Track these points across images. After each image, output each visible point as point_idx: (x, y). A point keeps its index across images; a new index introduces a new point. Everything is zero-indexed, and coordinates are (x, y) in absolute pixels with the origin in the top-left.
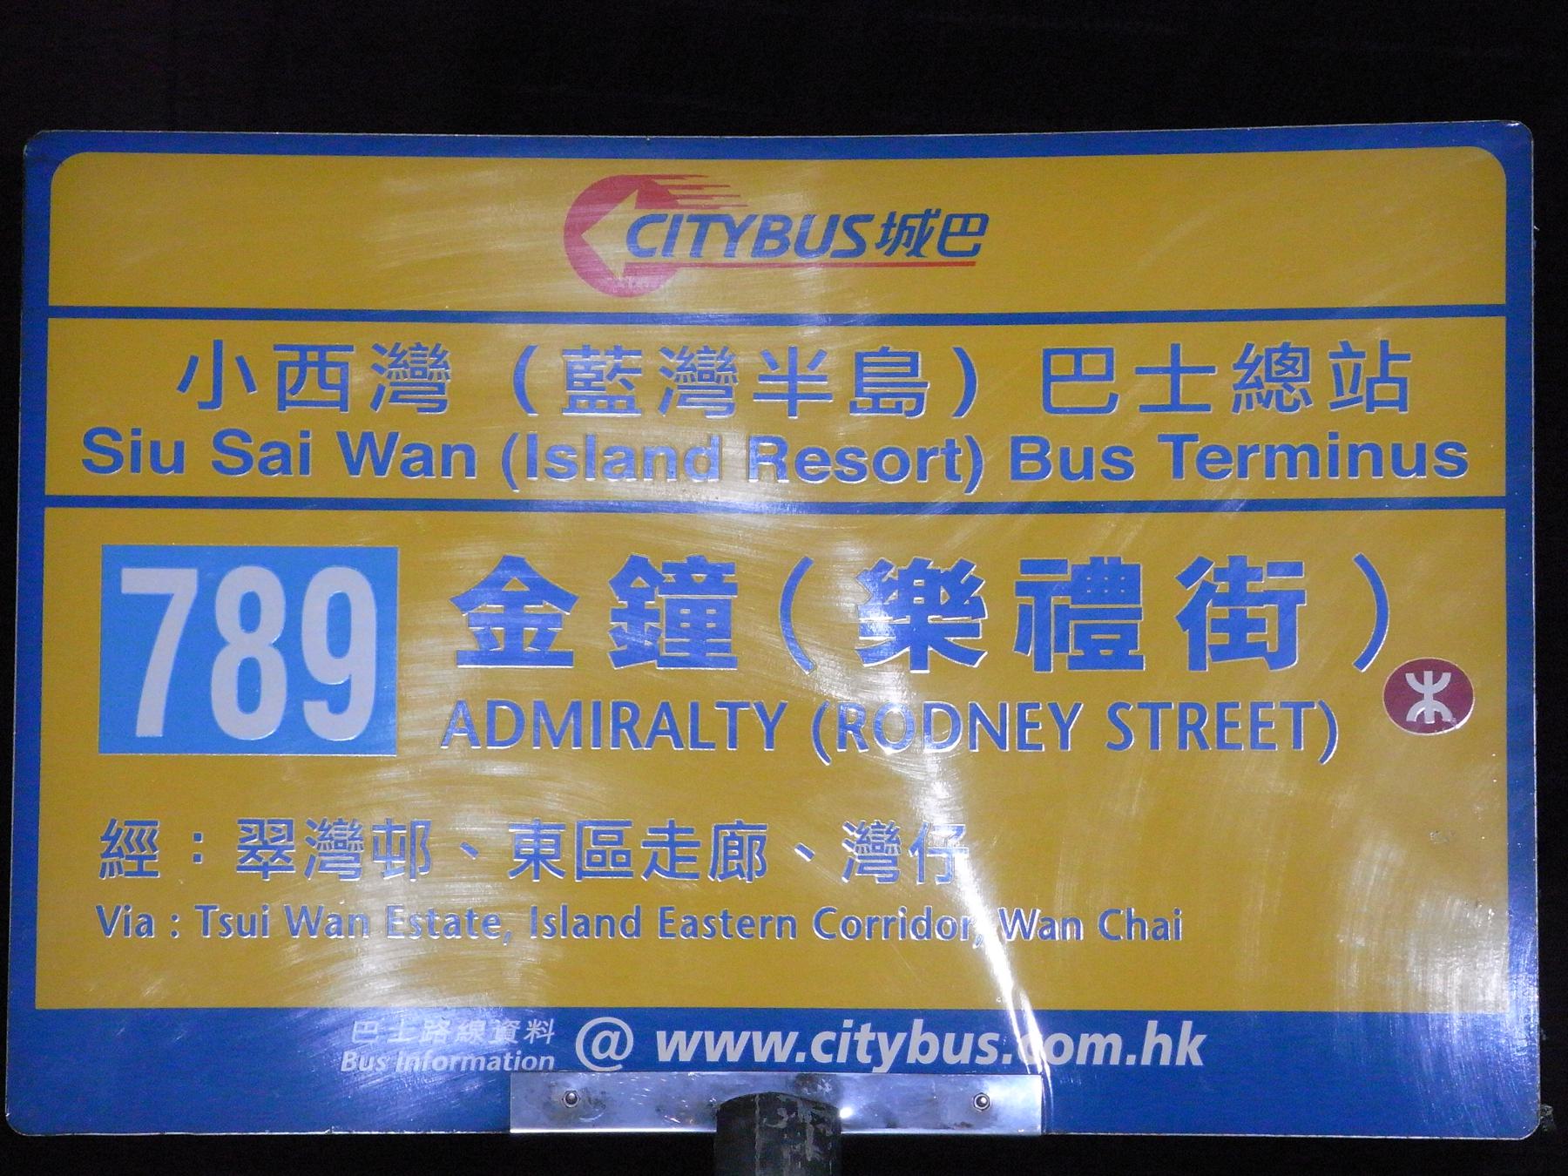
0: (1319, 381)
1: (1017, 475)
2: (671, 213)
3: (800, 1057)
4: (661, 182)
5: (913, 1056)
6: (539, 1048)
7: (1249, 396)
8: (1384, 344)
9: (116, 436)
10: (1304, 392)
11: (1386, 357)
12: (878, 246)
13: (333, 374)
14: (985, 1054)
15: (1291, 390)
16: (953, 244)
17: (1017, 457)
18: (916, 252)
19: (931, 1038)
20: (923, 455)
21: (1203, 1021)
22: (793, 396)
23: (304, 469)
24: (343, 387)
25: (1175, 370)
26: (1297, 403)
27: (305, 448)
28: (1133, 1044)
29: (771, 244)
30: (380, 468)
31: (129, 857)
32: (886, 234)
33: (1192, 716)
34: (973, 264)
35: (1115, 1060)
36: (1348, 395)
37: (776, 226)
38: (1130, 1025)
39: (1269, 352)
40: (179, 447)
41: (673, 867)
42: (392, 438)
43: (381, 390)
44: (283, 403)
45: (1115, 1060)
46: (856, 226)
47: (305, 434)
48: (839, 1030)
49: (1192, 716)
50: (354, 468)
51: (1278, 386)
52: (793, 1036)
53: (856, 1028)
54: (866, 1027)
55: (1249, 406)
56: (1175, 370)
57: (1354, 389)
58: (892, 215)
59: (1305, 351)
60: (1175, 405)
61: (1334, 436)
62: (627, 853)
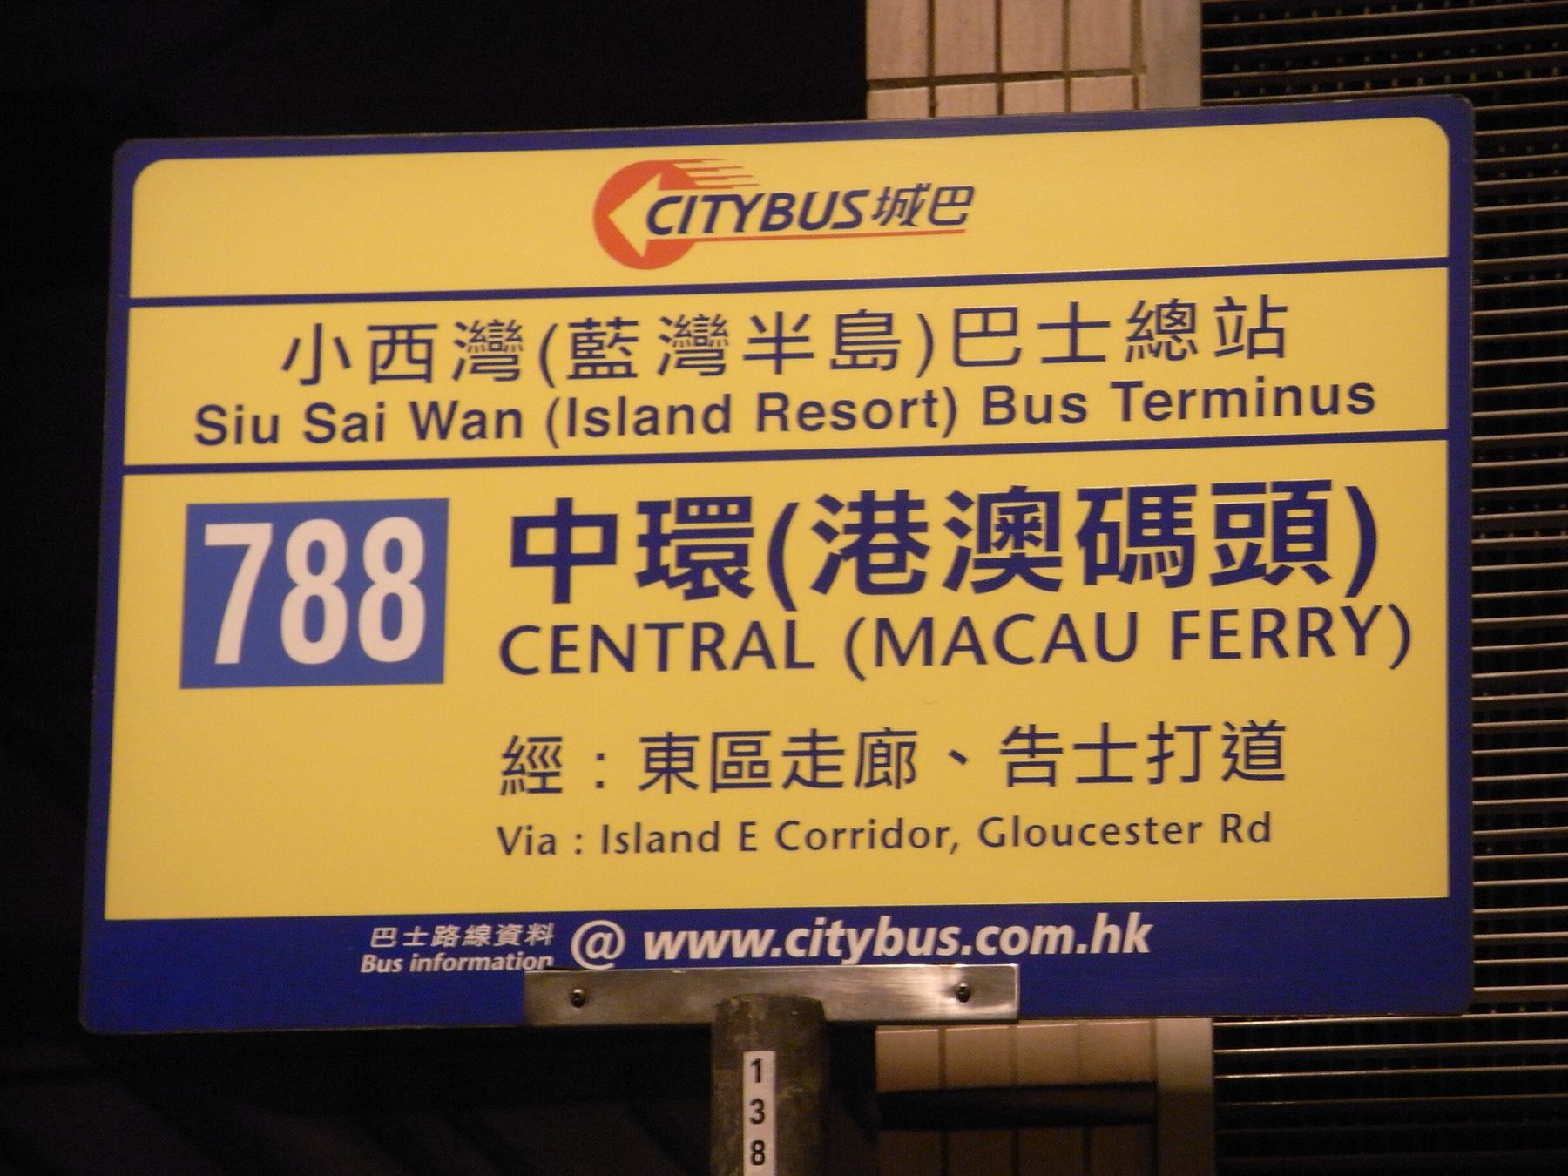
0: (1206, 335)
1: (988, 421)
2: (686, 194)
3: (776, 953)
4: (681, 166)
5: (880, 949)
6: (539, 950)
7: (1141, 348)
8: (1264, 298)
9: (222, 412)
10: (1190, 342)
11: (1266, 310)
12: (875, 217)
13: (419, 351)
14: (945, 946)
15: (1179, 340)
16: (942, 214)
17: (989, 405)
18: (908, 222)
19: (897, 933)
20: (906, 405)
21: (1149, 912)
22: (779, 357)
23: (380, 437)
24: (428, 361)
25: (1074, 326)
26: (1184, 352)
27: (381, 418)
28: (1084, 935)
29: (777, 219)
30: (443, 433)
31: (533, 775)
32: (881, 207)
33: (1269, 623)
34: (962, 231)
35: (1066, 950)
36: (1230, 345)
37: (781, 203)
38: (1080, 917)
39: (1160, 307)
40: (275, 419)
41: (815, 776)
42: (454, 405)
43: (462, 362)
44: (375, 378)
45: (1066, 950)
46: (855, 201)
47: (381, 405)
48: (812, 926)
49: (1269, 623)
50: (422, 434)
51: (1166, 338)
52: (770, 933)
53: (828, 926)
54: (837, 924)
55: (1141, 356)
56: (1074, 326)
57: (1236, 339)
58: (887, 190)
59: (1192, 306)
60: (1074, 357)
61: (1261, 379)
62: (765, 764)
